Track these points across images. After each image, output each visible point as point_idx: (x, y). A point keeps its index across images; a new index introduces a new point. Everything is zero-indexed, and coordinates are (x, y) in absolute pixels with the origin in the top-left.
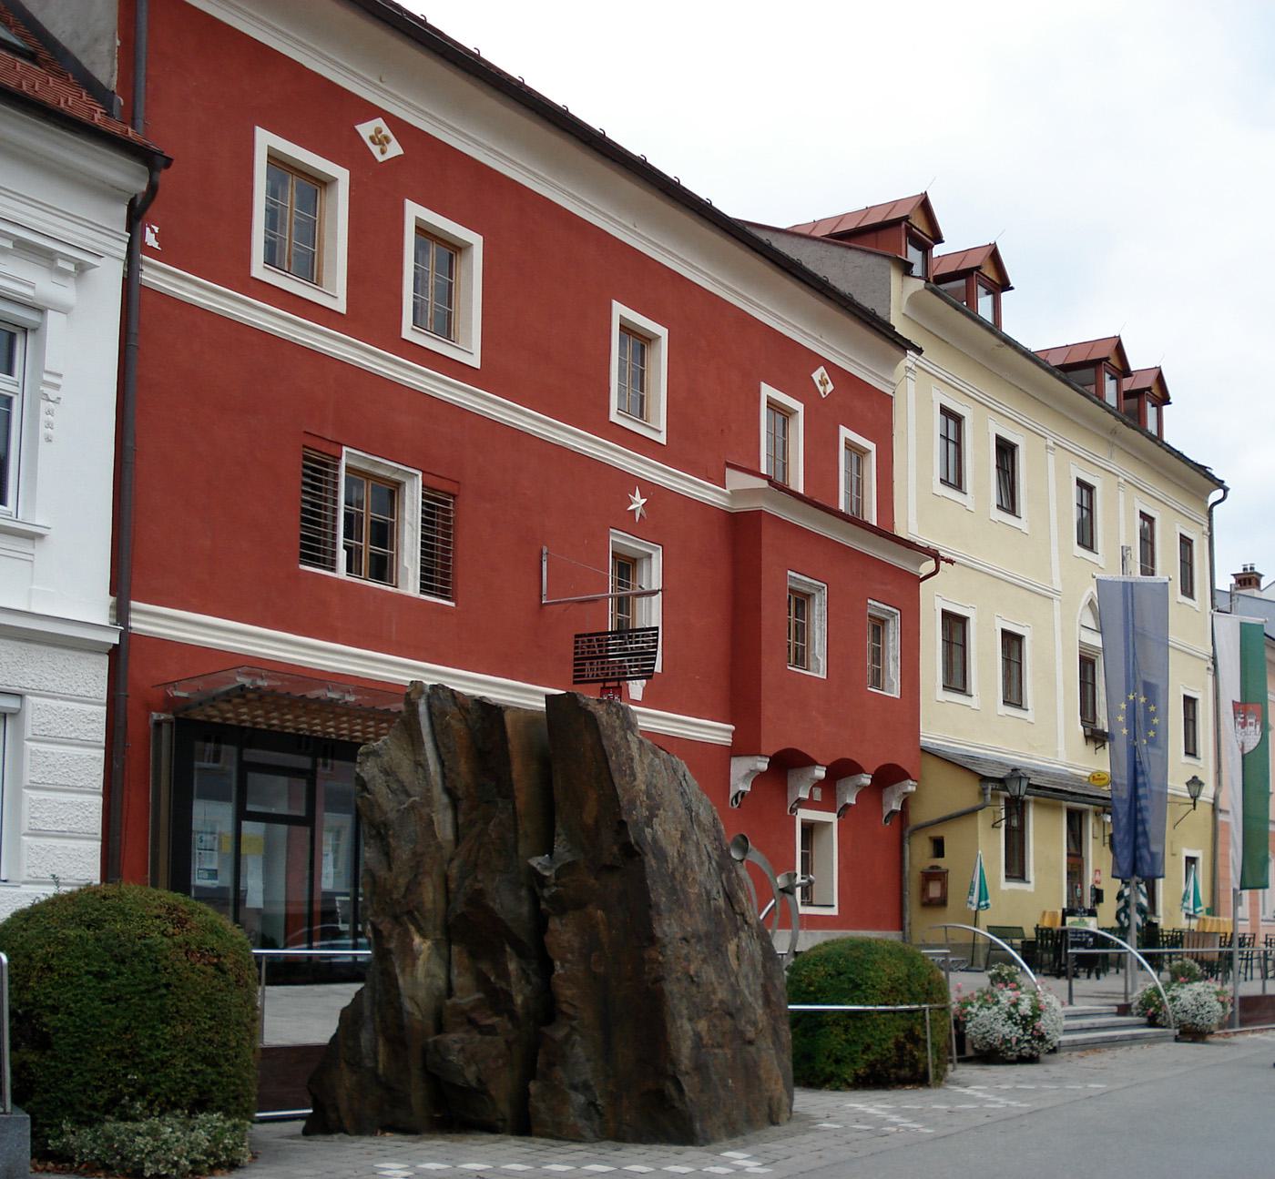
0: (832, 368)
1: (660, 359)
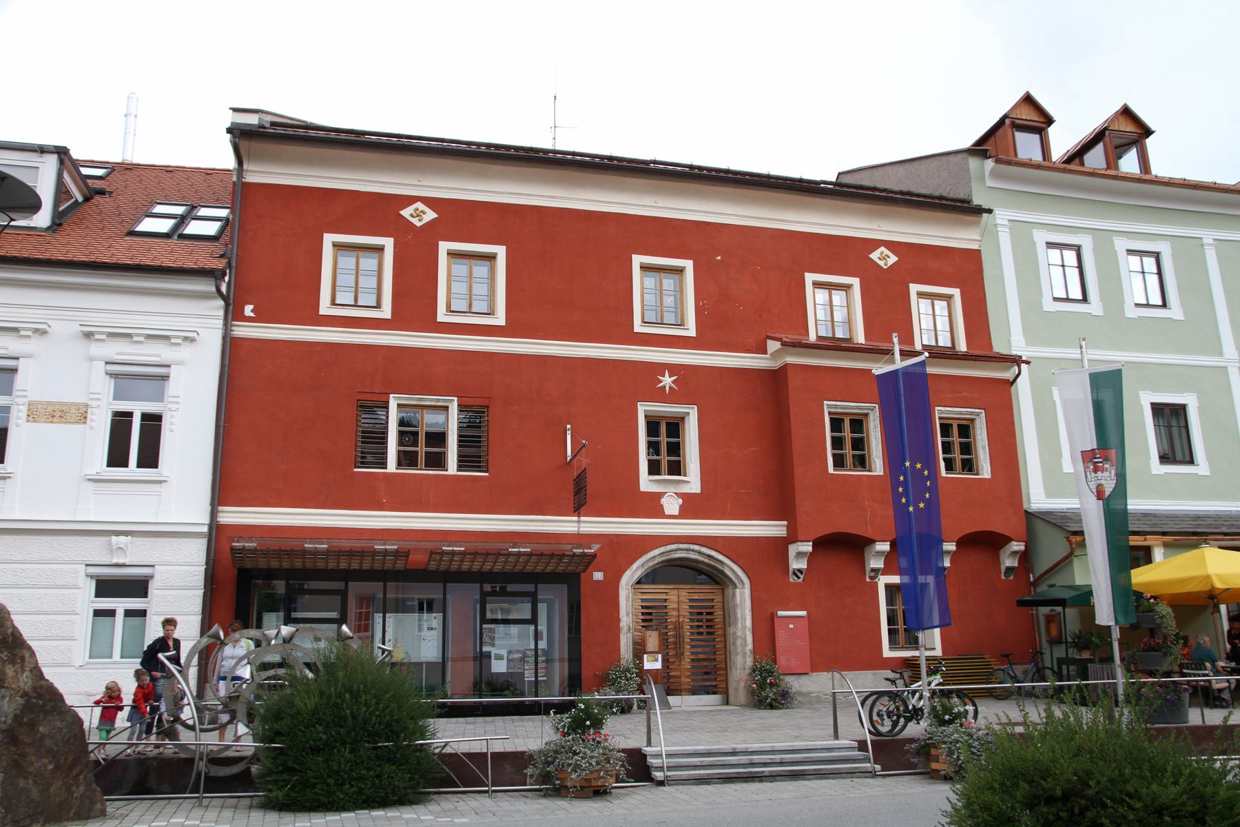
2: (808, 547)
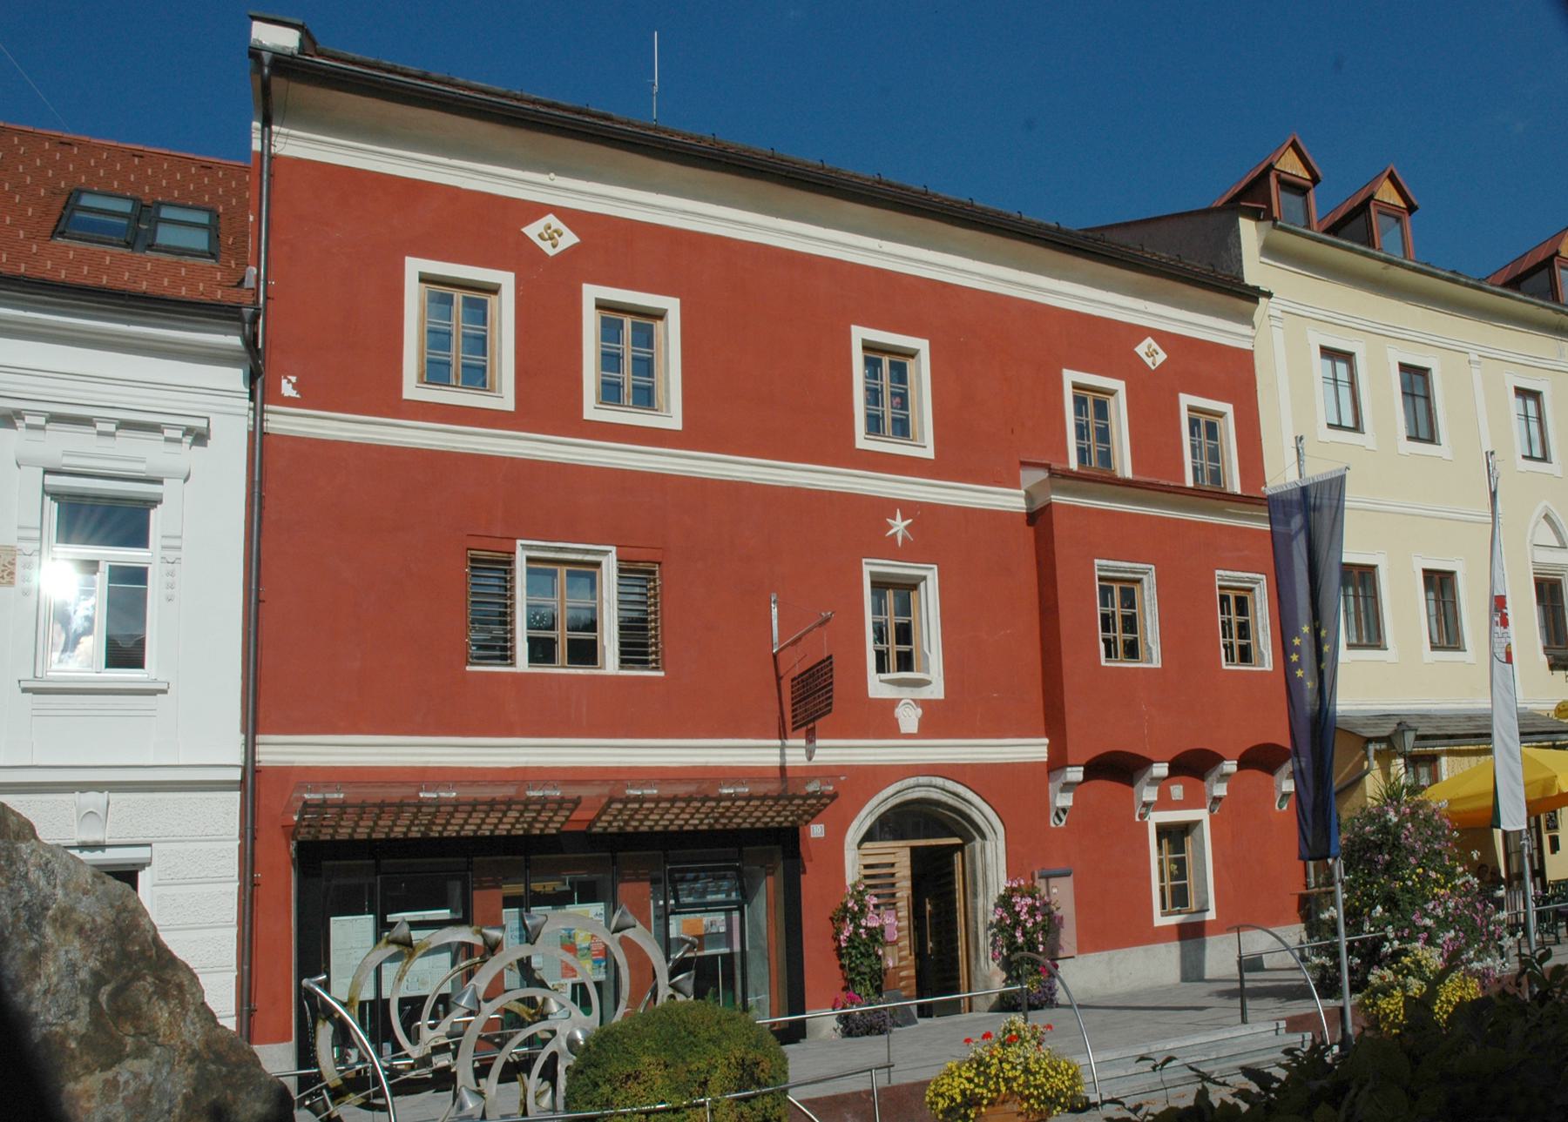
0: (1161, 337)
1: (921, 374)
2: (1075, 774)
